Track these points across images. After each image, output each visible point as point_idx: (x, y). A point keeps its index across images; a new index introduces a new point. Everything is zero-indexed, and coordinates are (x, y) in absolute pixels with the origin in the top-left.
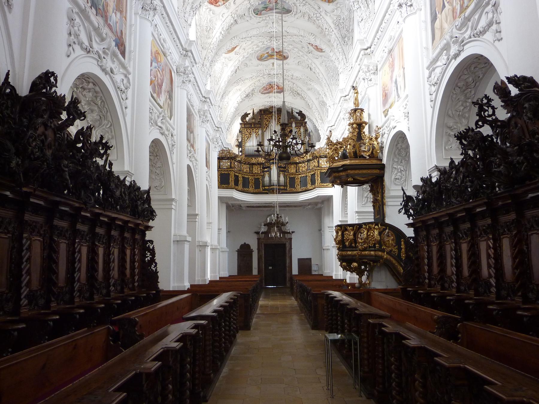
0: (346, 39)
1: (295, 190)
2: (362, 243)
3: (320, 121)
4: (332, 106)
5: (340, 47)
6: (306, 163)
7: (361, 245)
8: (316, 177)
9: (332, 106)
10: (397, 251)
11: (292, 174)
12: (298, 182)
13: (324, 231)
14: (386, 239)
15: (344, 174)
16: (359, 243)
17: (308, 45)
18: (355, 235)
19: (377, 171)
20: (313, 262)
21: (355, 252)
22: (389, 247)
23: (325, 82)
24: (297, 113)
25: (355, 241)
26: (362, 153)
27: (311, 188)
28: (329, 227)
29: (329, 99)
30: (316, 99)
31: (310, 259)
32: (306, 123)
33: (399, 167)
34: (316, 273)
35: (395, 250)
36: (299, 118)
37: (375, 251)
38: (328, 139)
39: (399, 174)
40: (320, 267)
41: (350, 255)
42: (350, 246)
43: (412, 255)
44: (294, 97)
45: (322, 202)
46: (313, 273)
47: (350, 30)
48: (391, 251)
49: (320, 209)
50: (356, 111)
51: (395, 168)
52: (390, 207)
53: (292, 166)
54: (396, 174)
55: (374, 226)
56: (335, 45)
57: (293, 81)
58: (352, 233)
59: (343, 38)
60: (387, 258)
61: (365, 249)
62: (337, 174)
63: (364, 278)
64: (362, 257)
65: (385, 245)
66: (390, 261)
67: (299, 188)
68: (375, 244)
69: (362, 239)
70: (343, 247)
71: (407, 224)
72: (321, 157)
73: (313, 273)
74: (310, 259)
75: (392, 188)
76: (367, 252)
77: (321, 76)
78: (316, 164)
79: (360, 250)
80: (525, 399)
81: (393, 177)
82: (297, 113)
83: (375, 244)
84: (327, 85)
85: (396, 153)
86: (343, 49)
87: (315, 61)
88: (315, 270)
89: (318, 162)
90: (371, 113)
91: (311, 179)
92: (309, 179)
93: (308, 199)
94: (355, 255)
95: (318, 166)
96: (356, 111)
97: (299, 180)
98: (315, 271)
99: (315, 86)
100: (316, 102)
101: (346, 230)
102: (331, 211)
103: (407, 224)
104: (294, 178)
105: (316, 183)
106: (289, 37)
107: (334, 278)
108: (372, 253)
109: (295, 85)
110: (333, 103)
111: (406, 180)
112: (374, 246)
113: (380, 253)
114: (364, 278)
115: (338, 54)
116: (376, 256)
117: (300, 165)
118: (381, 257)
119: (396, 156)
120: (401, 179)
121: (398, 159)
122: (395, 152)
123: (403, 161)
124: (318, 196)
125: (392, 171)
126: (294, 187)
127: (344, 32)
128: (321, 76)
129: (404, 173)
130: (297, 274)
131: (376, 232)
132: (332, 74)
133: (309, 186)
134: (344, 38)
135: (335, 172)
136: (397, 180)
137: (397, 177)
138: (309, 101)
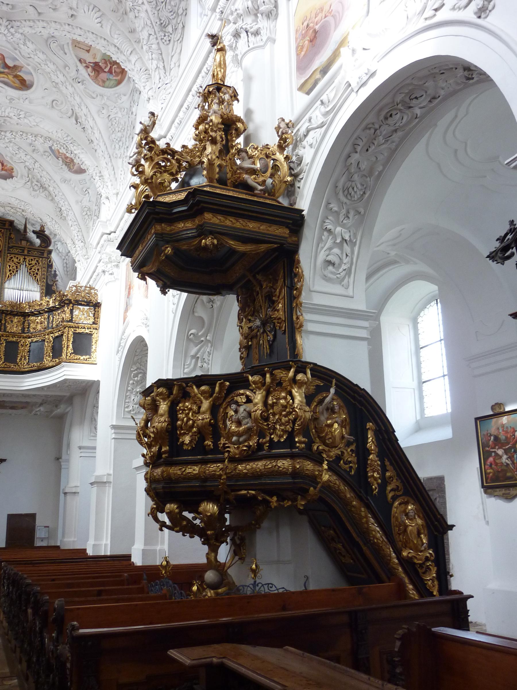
0: (170, 29)
1: (16, 368)
2: (239, 435)
3: (79, 244)
4: (113, 198)
5: (155, 41)
6: (46, 315)
7: (238, 443)
8: (65, 342)
9: (113, 198)
10: (353, 458)
11: (14, 335)
12: (23, 351)
13: (68, 461)
14: (325, 420)
15: (189, 225)
16: (230, 435)
17: (78, 63)
18: (214, 410)
19: (282, 232)
20: (39, 522)
21: (213, 468)
22: (333, 446)
23: (103, 148)
24: (34, 232)
25: (214, 429)
26: (245, 176)
27: (51, 364)
28: (80, 448)
29: (109, 184)
30: (77, 202)
31: (32, 517)
32: (50, 252)
33: (339, 229)
34: (44, 544)
35: (350, 456)
36: (38, 242)
37: (292, 456)
38: (146, 131)
39: (336, 250)
40: (52, 531)
41: (196, 477)
42: (199, 447)
43: (186, 514)
44: (33, 193)
45: (70, 400)
46: (38, 543)
47: (180, 11)
48: (339, 458)
49: (61, 419)
50: (217, 90)
51: (329, 231)
52: (312, 337)
53: (15, 320)
54: (330, 249)
55: (291, 373)
56: (144, 35)
57: (35, 155)
58: (206, 405)
59: (163, 26)
60: (329, 481)
61: (251, 455)
62: (167, 228)
63: (224, 553)
64: (237, 481)
65: (323, 441)
66: (337, 493)
67: (24, 364)
68: (291, 435)
69: (239, 423)
70: (172, 453)
71: (511, 315)
72: (78, 303)
73: (38, 543)
74: (32, 517)
75: (317, 288)
76: (260, 465)
77: (97, 135)
78: (67, 316)
79: (233, 460)
80: (215, 660)
81: (322, 256)
82: (34, 232)
83: (291, 435)
84: (107, 156)
85: (340, 185)
86: (160, 49)
87: (88, 101)
88: (41, 538)
89: (72, 311)
90: (252, 106)
91: (53, 348)
92: (48, 346)
93: (42, 388)
94: (214, 477)
95: (71, 321)
96: (217, 90)
97: (27, 348)
98: (42, 540)
99: (81, 156)
100: (76, 209)
101: (185, 395)
102: (89, 411)
103: (511, 315)
104: (17, 343)
105: (64, 356)
106: (41, 24)
107: (137, 560)
108: (284, 464)
109: (37, 165)
110: (115, 191)
111: (350, 269)
112: (290, 442)
113: (309, 466)
114: (224, 553)
115: (147, 56)
116: (295, 474)
117: (32, 318)
118: (314, 479)
119: (337, 194)
120: (340, 265)
121: (341, 204)
122: (337, 181)
123: (351, 215)
124: (65, 380)
125: (320, 240)
126: (15, 362)
127: (165, 14)
128: (97, 135)
129: (347, 248)
130: (426, 416)
131: (298, 396)
132: (119, 134)
133: (47, 361)
134: (165, 27)
135: (160, 221)
136: (331, 268)
137: (330, 258)
138: (61, 202)
